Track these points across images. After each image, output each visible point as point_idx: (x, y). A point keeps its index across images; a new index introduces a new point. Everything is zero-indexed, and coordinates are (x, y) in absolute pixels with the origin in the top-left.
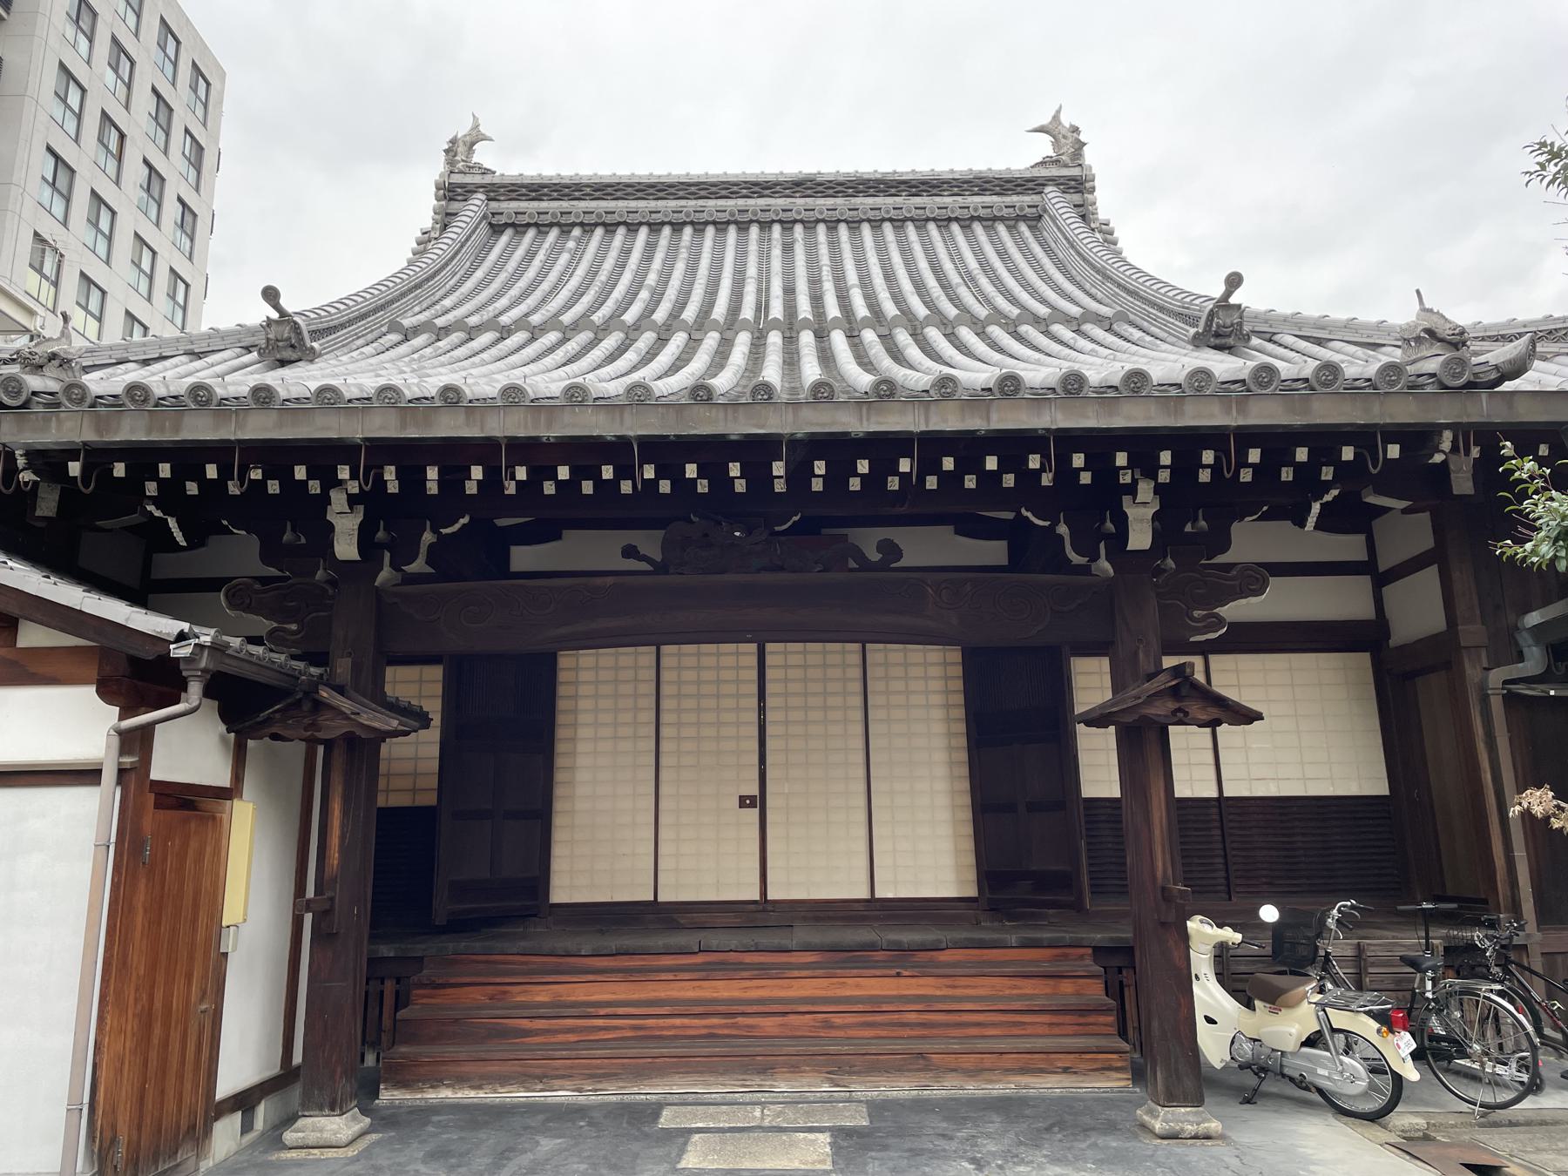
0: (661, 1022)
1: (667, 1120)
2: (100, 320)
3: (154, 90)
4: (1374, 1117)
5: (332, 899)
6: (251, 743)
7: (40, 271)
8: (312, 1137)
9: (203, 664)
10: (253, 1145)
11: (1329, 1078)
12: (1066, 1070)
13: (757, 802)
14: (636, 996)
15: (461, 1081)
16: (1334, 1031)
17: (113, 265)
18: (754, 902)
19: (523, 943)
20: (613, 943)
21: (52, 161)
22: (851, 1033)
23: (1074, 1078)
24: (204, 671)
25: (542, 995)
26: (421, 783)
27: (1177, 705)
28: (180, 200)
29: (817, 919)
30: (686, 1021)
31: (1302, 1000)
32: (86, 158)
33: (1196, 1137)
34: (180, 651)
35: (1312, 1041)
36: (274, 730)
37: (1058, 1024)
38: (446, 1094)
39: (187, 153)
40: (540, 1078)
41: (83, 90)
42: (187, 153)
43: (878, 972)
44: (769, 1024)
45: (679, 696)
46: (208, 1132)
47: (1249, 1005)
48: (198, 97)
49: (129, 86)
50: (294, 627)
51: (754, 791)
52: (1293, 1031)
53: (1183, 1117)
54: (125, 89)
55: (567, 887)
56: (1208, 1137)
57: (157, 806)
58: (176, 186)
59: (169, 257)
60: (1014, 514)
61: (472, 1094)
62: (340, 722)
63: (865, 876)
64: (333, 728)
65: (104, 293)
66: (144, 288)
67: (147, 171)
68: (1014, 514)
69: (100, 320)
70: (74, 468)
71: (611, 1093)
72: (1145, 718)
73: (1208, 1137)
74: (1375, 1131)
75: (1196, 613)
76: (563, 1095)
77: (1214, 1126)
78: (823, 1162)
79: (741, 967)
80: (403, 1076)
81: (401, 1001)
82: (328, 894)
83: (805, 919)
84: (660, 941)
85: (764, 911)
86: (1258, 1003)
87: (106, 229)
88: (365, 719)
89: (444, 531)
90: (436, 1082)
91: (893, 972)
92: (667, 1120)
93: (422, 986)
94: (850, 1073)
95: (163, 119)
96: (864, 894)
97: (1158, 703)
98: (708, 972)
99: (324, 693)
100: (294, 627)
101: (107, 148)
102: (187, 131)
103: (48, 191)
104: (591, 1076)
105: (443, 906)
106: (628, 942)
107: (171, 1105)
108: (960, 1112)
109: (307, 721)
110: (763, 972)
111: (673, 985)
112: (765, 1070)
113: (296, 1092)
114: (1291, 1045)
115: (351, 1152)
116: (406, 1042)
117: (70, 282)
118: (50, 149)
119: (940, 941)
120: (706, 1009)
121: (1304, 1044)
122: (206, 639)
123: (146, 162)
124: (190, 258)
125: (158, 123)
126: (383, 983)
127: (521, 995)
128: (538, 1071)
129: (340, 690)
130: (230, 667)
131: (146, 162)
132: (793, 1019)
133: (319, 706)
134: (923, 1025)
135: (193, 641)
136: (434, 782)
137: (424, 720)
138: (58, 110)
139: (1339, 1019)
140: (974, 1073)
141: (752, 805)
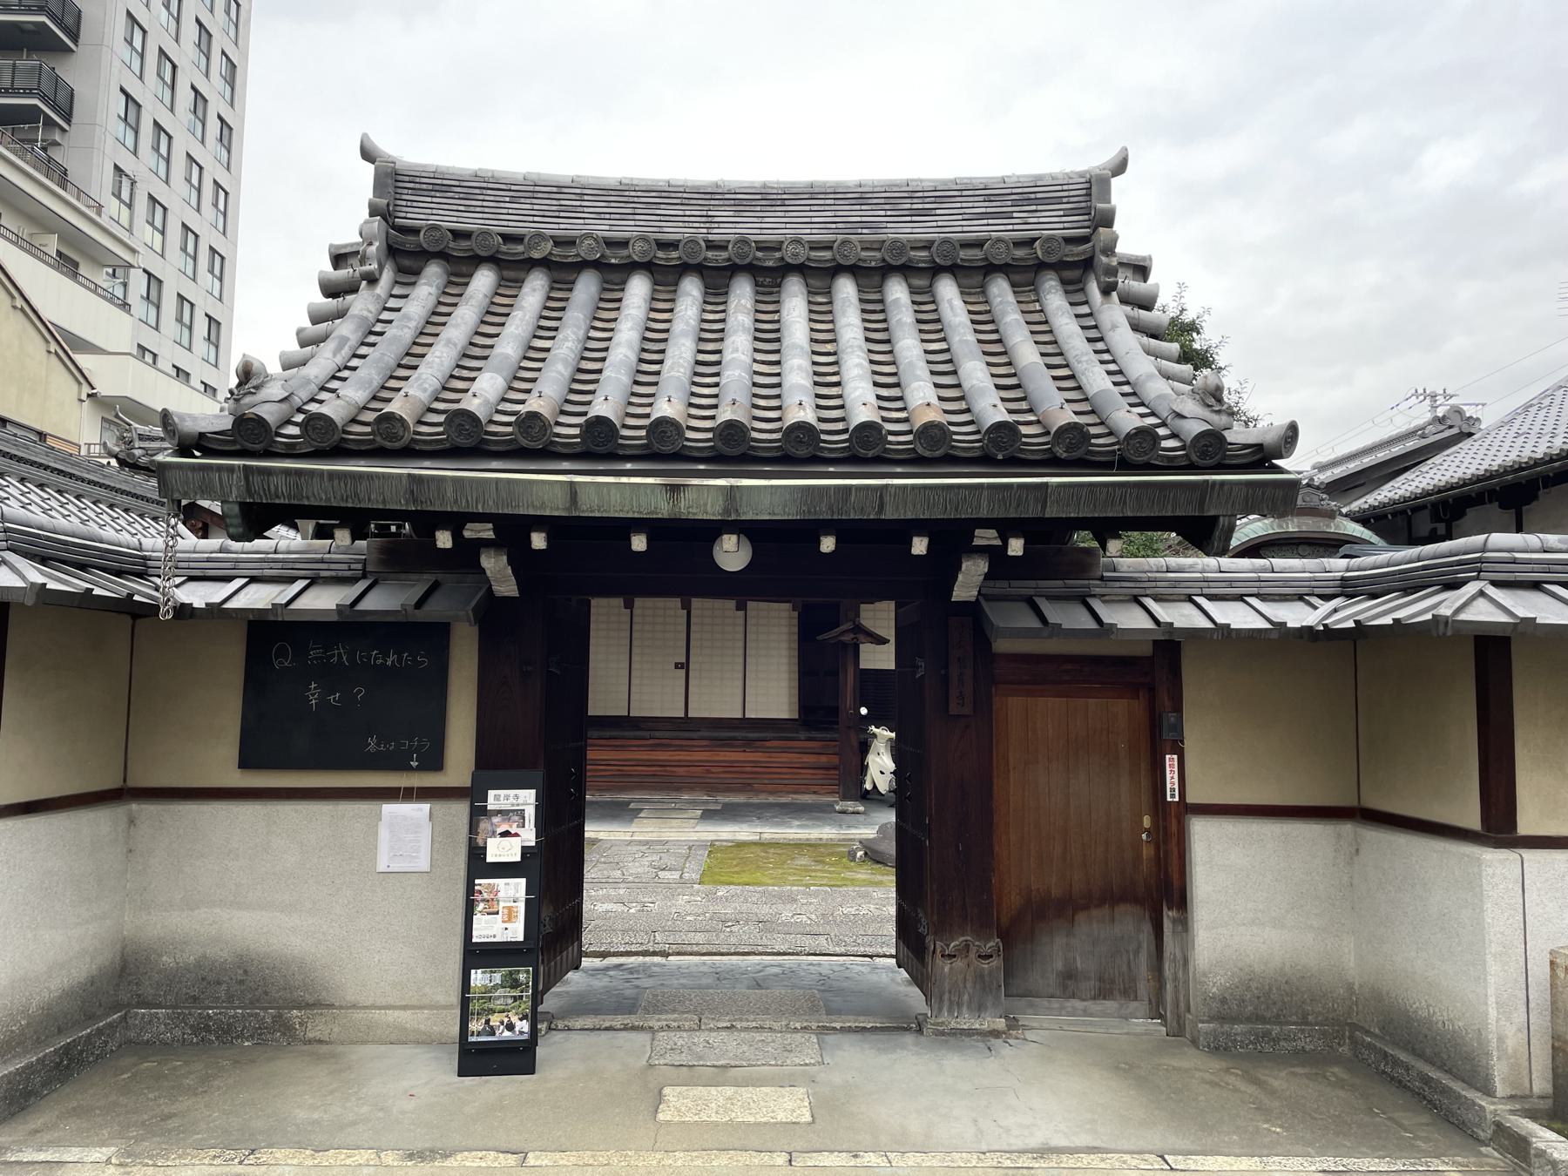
1: (632, 806)
2: (163, 233)
3: (198, 21)
7: (152, 224)
12: (815, 793)
13: (685, 666)
17: (172, 184)
20: (608, 734)
21: (123, 98)
28: (220, 117)
32: (148, 93)
33: (853, 813)
39: (223, 73)
41: (144, 32)
42: (223, 73)
44: (681, 771)
48: (230, 19)
49: (178, 21)
51: (684, 661)
53: (850, 805)
54: (175, 23)
56: (858, 813)
58: (216, 106)
59: (214, 171)
60: (467, 534)
65: (165, 209)
66: (130, 142)
67: (193, 94)
68: (467, 534)
69: (163, 233)
70: (538, 541)
73: (858, 813)
77: (861, 809)
84: (631, 734)
87: (164, 153)
92: (632, 806)
95: (204, 48)
96: (739, 716)
98: (654, 747)
101: (163, 79)
102: (223, 53)
103: (122, 125)
106: (615, 733)
110: (681, 748)
112: (678, 789)
117: (141, 204)
118: (122, 90)
120: (651, 763)
123: (193, 87)
124: (228, 169)
125: (201, 50)
131: (193, 87)
138: (125, 52)
140: (771, 793)
141: (682, 668)
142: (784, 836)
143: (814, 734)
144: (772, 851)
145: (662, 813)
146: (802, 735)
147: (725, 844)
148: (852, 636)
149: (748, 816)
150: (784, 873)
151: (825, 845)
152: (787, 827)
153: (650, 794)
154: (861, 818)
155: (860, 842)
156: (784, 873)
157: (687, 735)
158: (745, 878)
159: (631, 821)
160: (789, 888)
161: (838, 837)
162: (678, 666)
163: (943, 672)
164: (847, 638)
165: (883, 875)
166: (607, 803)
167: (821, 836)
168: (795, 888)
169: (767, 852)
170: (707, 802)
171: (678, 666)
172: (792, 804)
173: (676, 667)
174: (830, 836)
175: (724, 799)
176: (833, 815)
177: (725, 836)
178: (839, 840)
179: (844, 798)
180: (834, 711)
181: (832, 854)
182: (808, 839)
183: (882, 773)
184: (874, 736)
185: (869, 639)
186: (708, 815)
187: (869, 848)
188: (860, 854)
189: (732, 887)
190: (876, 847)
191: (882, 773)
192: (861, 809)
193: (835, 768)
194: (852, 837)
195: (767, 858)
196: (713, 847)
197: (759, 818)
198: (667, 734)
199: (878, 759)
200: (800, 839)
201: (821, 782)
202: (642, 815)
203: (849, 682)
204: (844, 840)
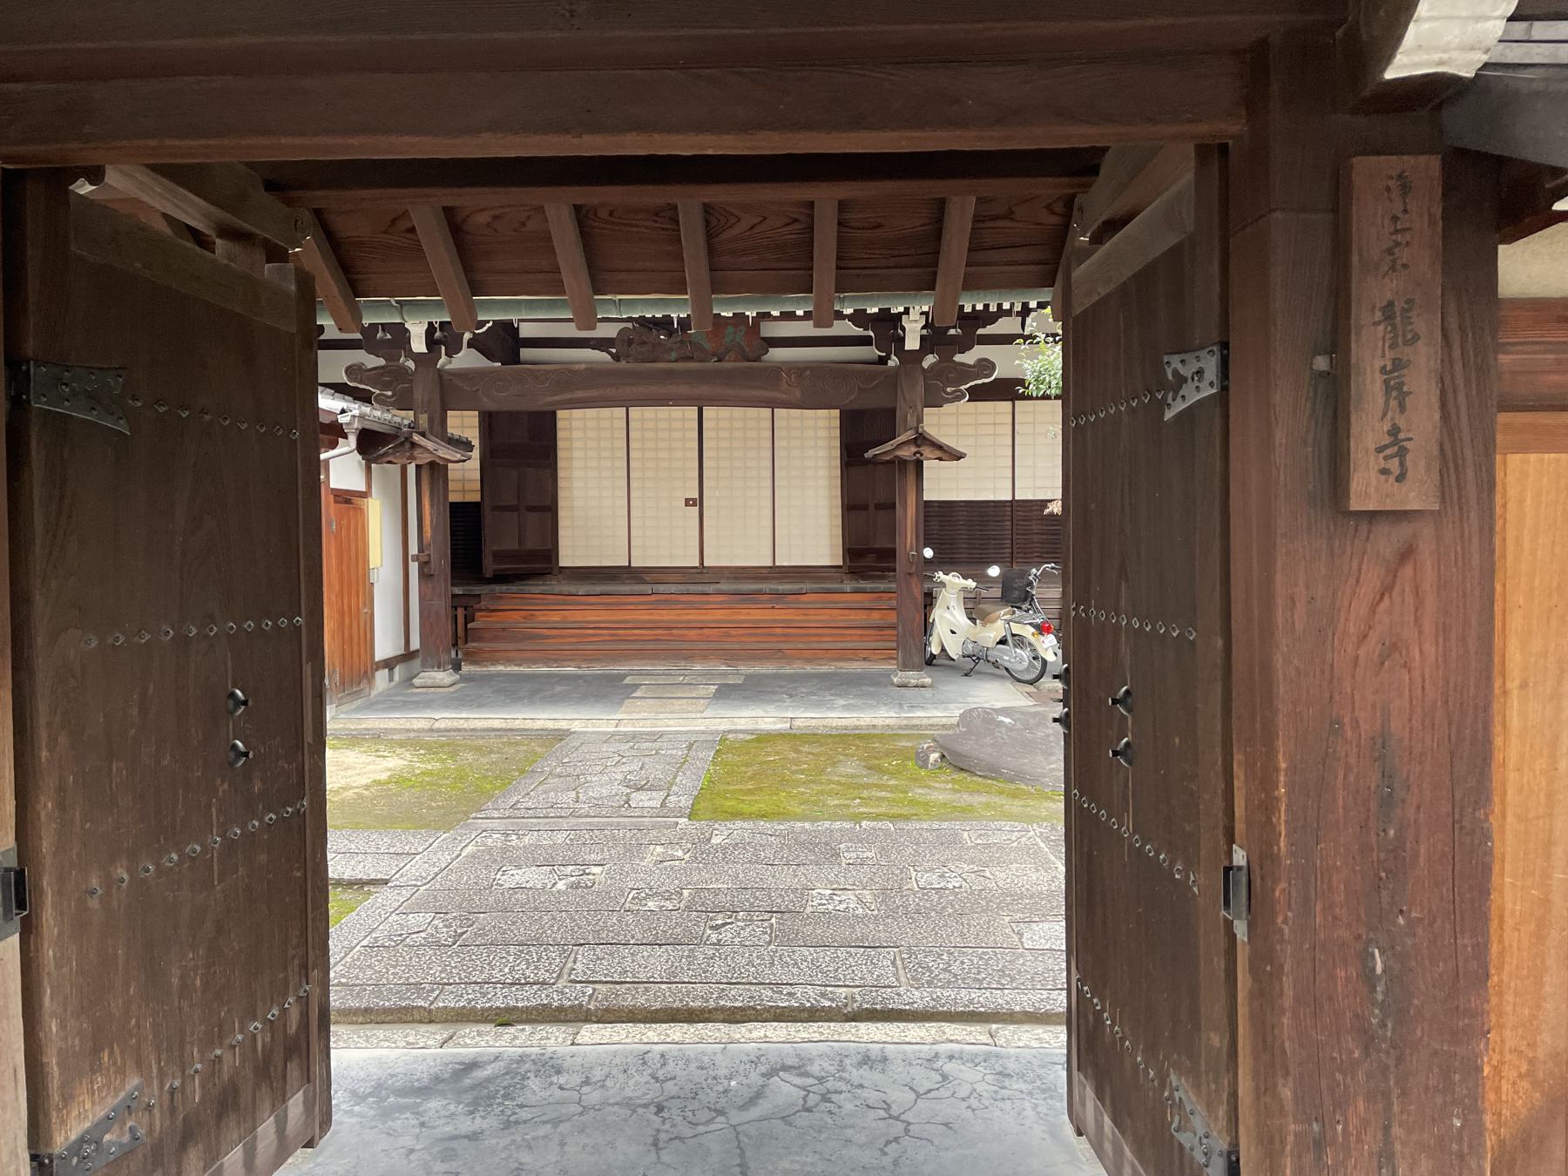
0: (628, 632)
1: (628, 681)
4: (1031, 683)
5: (429, 555)
6: (373, 465)
8: (429, 682)
9: (355, 426)
10: (394, 687)
11: (1009, 661)
12: (865, 659)
13: (698, 502)
14: (613, 618)
15: (509, 661)
16: (1013, 635)
18: (696, 568)
19: (542, 588)
20: (598, 589)
22: (743, 639)
23: (870, 663)
24: (356, 429)
25: (555, 617)
26: (468, 487)
27: (916, 450)
29: (736, 578)
30: (642, 632)
31: (997, 620)
34: (343, 419)
35: (1003, 642)
36: (389, 459)
37: (865, 635)
38: (500, 668)
40: (556, 661)
43: (761, 606)
45: (643, 429)
46: (373, 676)
47: (973, 620)
50: (390, 393)
51: (696, 496)
52: (992, 635)
53: (912, 677)
55: (569, 557)
57: (336, 502)
61: (516, 668)
62: (426, 455)
63: (770, 552)
64: (424, 459)
71: (597, 669)
72: (897, 457)
74: (1030, 689)
75: (949, 390)
76: (570, 670)
77: (928, 680)
78: (1060, 1048)
79: (678, 602)
80: (473, 658)
81: (469, 619)
82: (427, 552)
83: (728, 578)
85: (701, 573)
86: (978, 621)
88: (440, 453)
89: (477, 332)
90: (495, 662)
91: (770, 606)
92: (628, 681)
93: (480, 610)
94: (738, 660)
97: (906, 448)
99: (416, 438)
100: (390, 393)
104: (585, 660)
105: (489, 567)
107: (356, 659)
108: (794, 678)
109: (408, 454)
110: (691, 606)
111: (635, 612)
113: (417, 662)
114: (991, 644)
115: (451, 689)
116: (473, 641)
119: (801, 589)
121: (998, 643)
122: (356, 412)
126: (456, 610)
127: (541, 617)
128: (554, 657)
129: (423, 434)
130: (368, 426)
132: (706, 631)
133: (414, 445)
134: (784, 635)
135: (350, 414)
136: (478, 486)
137: (468, 446)
139: (1016, 629)
140: (808, 661)
142: (825, 722)
143: (863, 584)
144: (806, 748)
145: (664, 691)
146: (848, 586)
147: (741, 736)
148: (914, 449)
149: (775, 693)
150: (822, 792)
151: (880, 737)
152: (828, 709)
153: (653, 665)
154: (927, 693)
155: (934, 740)
156: (822, 792)
157: (699, 588)
158: (761, 803)
159: (620, 703)
160: (827, 824)
161: (899, 722)
162: (688, 502)
163: (1321, 363)
164: (907, 453)
165: (972, 793)
166: (597, 677)
167: (875, 722)
168: (837, 825)
169: (798, 751)
170: (724, 674)
171: (688, 502)
172: (836, 674)
173: (687, 504)
174: (887, 722)
175: (746, 669)
176: (890, 688)
177: (742, 724)
178: (900, 728)
179: (905, 666)
180: (889, 555)
181: (888, 754)
182: (856, 728)
183: (953, 632)
184: (943, 584)
185: (939, 454)
186: (726, 693)
187: (947, 749)
188: (934, 756)
189: (739, 824)
190: (959, 748)
191: (953, 632)
192: (928, 680)
193: (893, 627)
194: (917, 722)
195: (797, 762)
196: (724, 744)
197: (791, 696)
198: (673, 588)
199: (947, 615)
200: (846, 728)
201: (873, 645)
202: (637, 694)
203: (909, 516)
204: (907, 727)
